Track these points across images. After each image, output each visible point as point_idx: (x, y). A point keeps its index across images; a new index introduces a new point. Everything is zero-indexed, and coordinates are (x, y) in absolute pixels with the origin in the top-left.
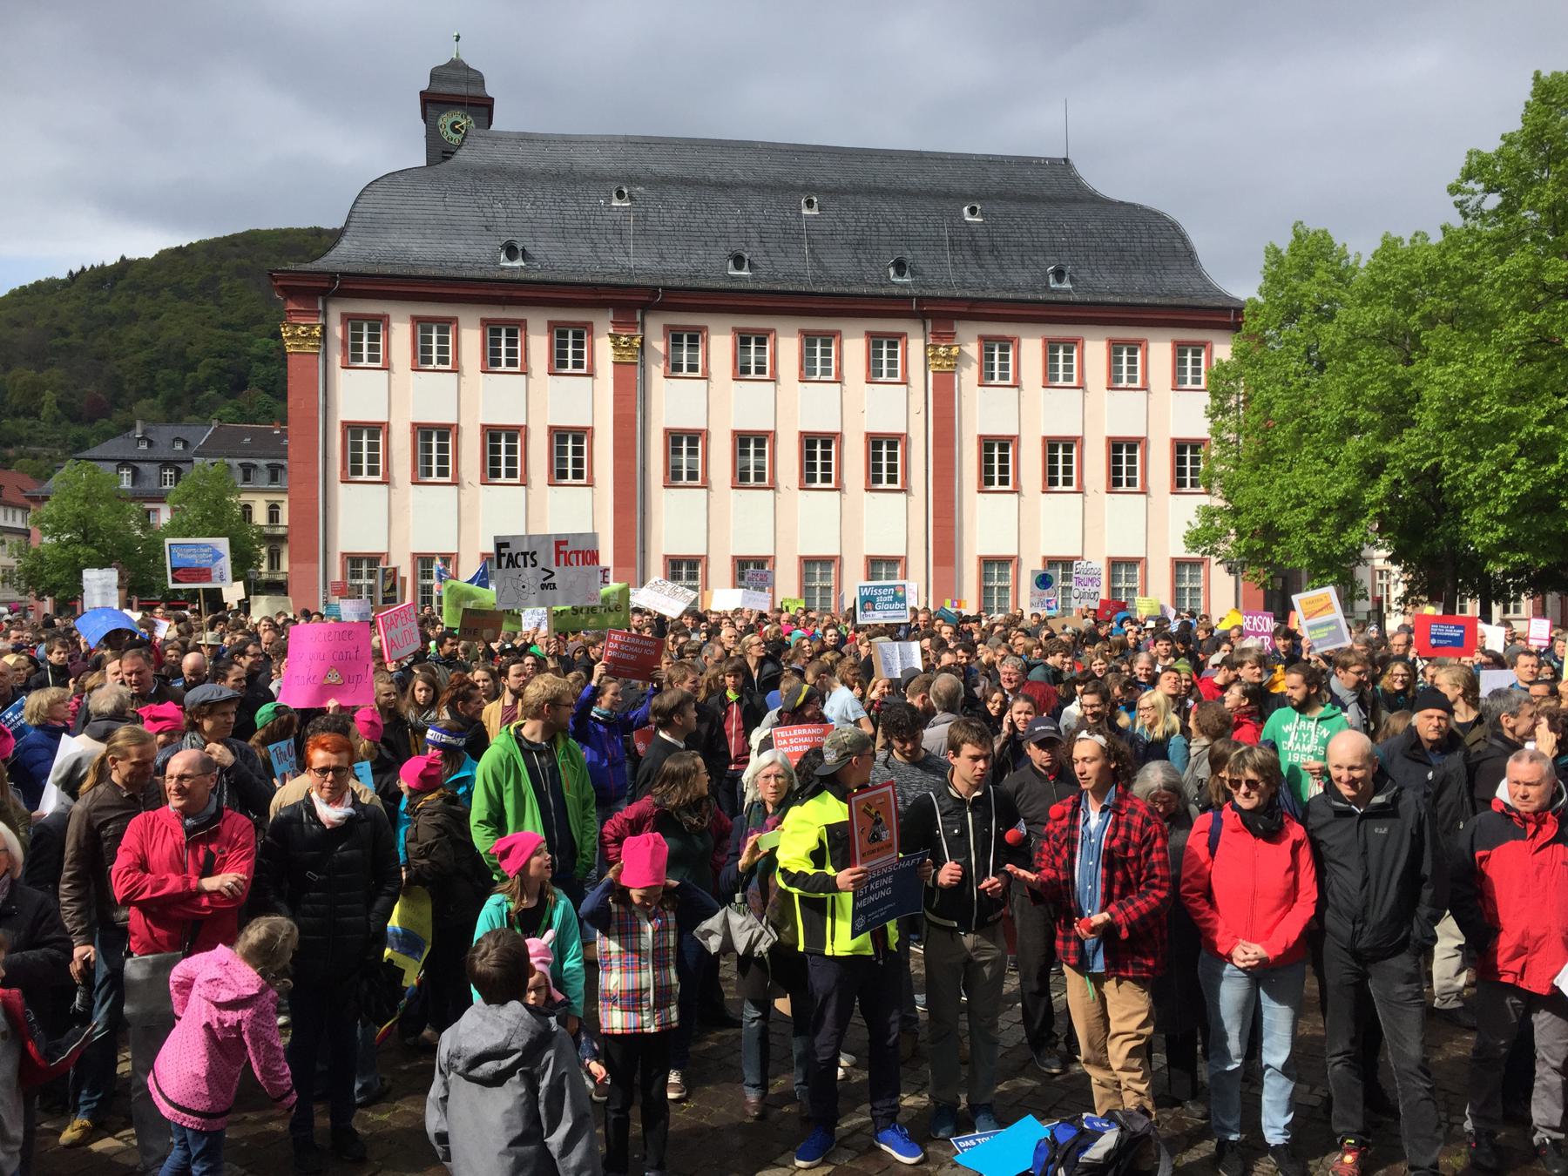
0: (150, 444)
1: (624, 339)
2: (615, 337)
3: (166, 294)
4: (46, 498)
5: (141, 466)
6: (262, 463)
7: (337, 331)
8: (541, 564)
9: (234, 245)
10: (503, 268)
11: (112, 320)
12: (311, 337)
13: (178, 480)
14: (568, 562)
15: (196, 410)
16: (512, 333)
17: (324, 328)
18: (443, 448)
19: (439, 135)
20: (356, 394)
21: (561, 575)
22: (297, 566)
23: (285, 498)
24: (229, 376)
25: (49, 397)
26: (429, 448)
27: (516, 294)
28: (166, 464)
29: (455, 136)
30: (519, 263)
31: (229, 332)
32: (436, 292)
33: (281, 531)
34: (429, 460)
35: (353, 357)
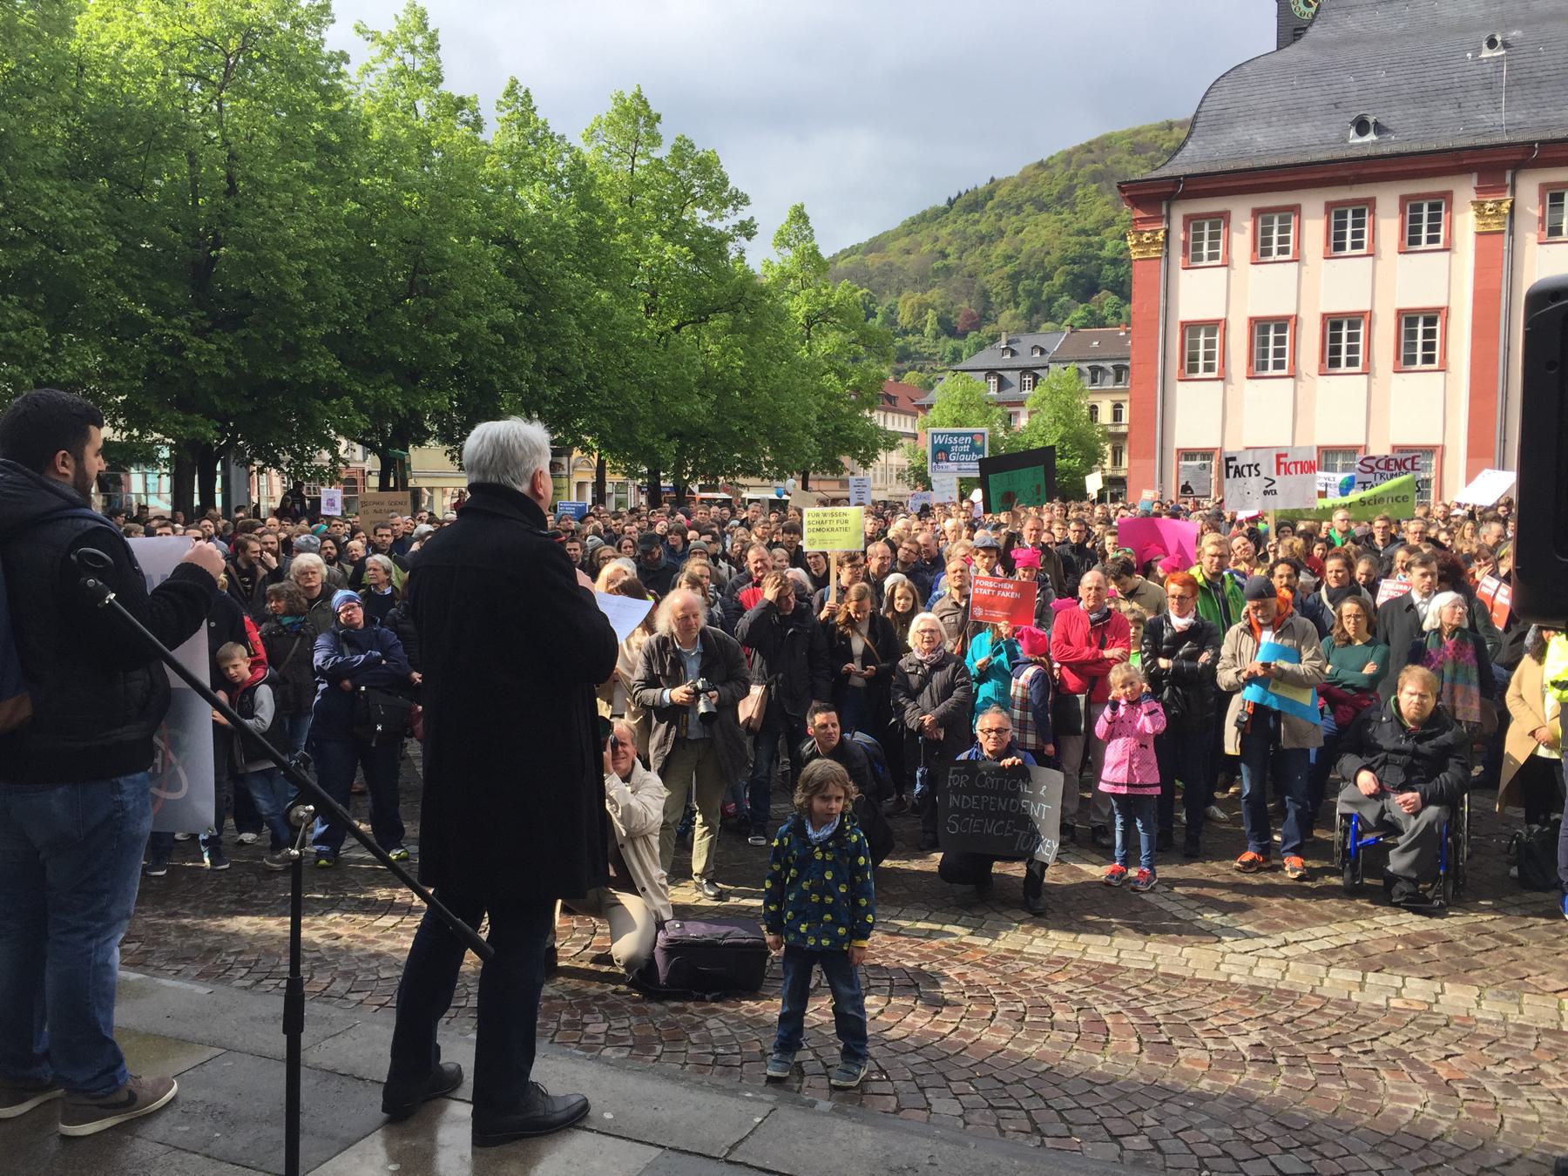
0: (1013, 353)
1: (1488, 206)
2: (1479, 205)
3: (1028, 208)
4: (930, 406)
5: (1006, 374)
6: (1108, 365)
7: (1179, 235)
8: (1264, 473)
9: (1090, 151)
10: (1352, 146)
11: (982, 239)
12: (1155, 242)
13: (1035, 385)
14: (1287, 471)
15: (1051, 318)
16: (1358, 213)
17: (1167, 232)
18: (1429, 334)
19: (1291, 13)
20: (1197, 293)
21: (1281, 482)
22: (1136, 463)
23: (1126, 397)
24: (1082, 281)
25: (931, 315)
26: (1265, 342)
27: (1365, 171)
28: (1025, 371)
29: (1307, 10)
30: (1371, 137)
31: (1083, 239)
32: (1274, 182)
33: (1123, 429)
34: (1265, 354)
35: (1193, 256)
